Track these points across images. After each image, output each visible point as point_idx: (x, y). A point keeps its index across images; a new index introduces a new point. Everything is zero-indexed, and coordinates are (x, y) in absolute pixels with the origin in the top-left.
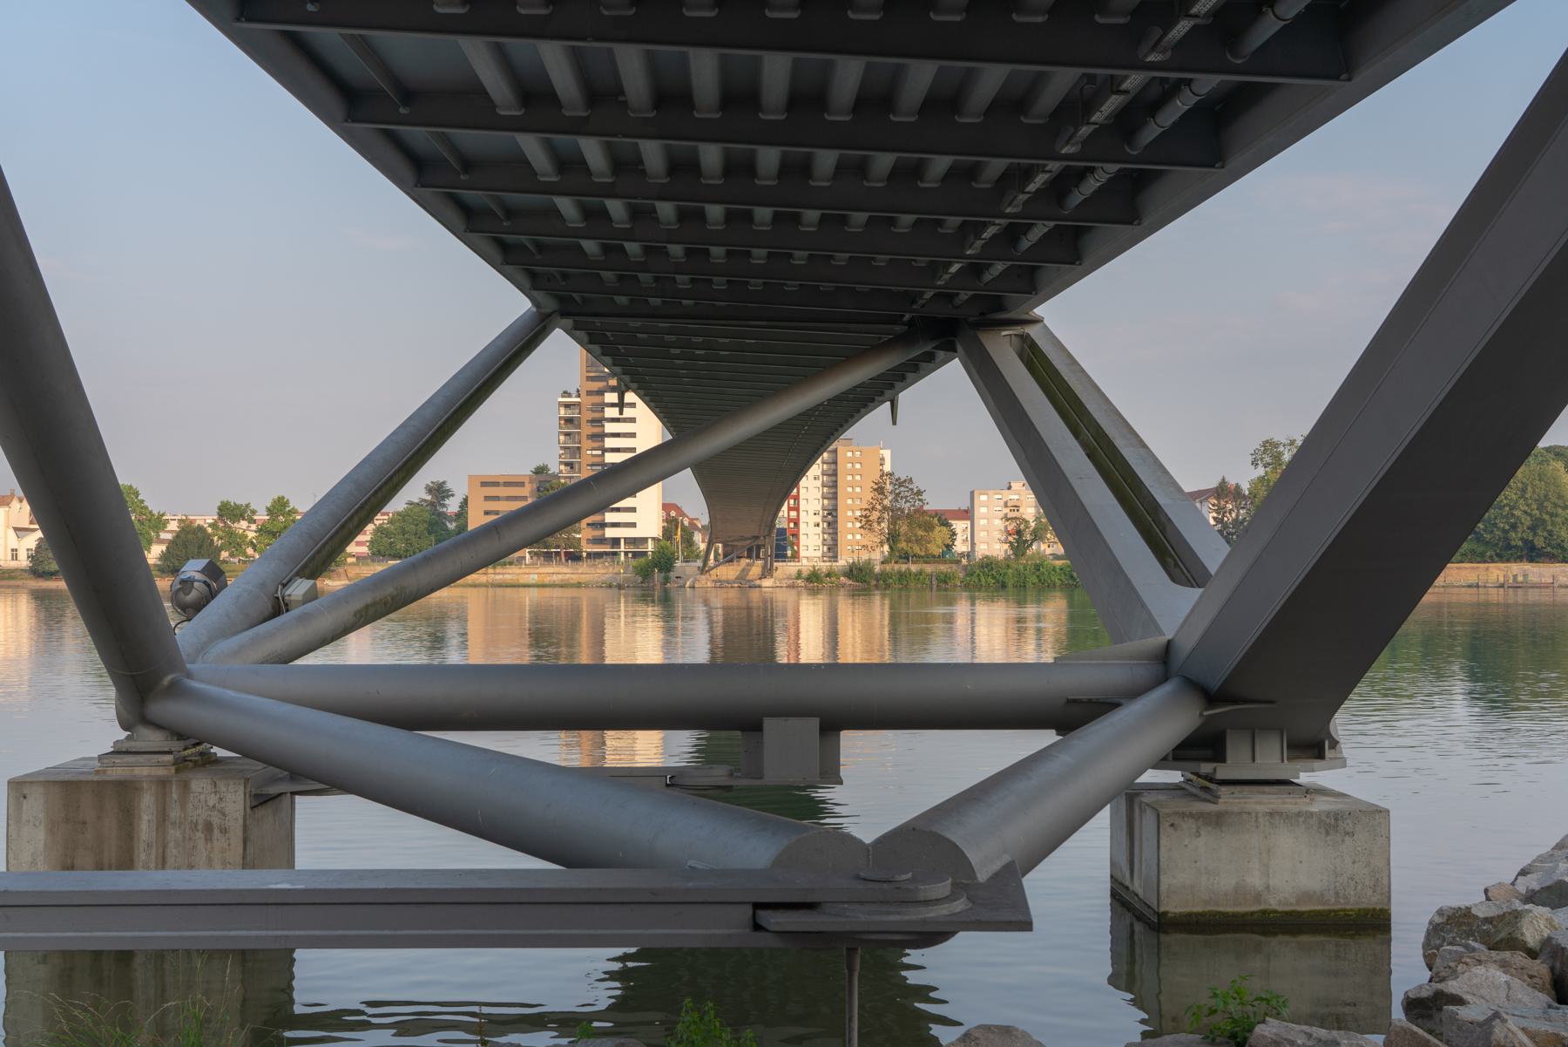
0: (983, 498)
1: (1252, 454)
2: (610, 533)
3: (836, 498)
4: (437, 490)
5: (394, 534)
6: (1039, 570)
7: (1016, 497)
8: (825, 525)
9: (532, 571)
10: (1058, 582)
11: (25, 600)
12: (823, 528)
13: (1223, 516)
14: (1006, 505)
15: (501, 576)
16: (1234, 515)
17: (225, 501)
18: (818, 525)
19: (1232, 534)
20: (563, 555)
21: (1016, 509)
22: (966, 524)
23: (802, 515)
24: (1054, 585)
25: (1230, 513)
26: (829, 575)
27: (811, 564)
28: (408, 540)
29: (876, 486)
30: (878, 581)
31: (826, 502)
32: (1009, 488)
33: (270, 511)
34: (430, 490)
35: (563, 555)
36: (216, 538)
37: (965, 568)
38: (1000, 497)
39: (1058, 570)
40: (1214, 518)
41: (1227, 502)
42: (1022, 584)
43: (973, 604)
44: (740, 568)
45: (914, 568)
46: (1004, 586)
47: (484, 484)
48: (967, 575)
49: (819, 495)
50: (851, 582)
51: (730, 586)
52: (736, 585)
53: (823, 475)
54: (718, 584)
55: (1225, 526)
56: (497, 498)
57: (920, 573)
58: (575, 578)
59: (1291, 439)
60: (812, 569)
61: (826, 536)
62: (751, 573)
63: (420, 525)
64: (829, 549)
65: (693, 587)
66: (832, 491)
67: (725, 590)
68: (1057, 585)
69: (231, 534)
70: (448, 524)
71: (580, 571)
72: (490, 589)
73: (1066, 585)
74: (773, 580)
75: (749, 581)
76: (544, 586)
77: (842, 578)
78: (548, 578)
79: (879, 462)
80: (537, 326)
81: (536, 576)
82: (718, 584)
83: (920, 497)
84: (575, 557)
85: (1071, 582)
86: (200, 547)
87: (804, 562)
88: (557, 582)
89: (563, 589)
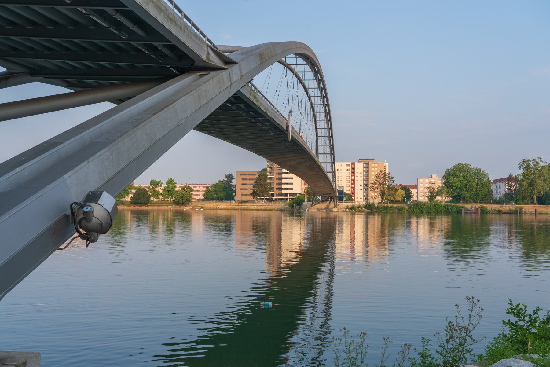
0: (422, 180)
1: (519, 164)
2: (284, 192)
3: (368, 180)
4: (229, 177)
5: (212, 192)
6: (436, 206)
7: (434, 180)
8: (364, 190)
9: (254, 205)
10: (443, 211)
11: (377, 216)
12: (364, 191)
13: (511, 187)
14: (430, 183)
15: (243, 206)
16: (515, 187)
17: (153, 179)
18: (362, 190)
19: (514, 194)
20: (265, 199)
21: (434, 184)
22: (416, 190)
23: (356, 186)
24: (441, 212)
25: (513, 187)
26: (358, 207)
27: (359, 203)
28: (216, 194)
29: (376, 176)
30: (376, 209)
31: (365, 182)
32: (431, 177)
33: (167, 183)
34: (227, 177)
35: (265, 199)
36: (149, 192)
37: (408, 205)
38: (428, 180)
39: (443, 207)
40: (507, 188)
41: (512, 183)
42: (429, 212)
43: (417, 219)
44: (327, 204)
45: (389, 205)
46: (422, 212)
47: (242, 174)
48: (409, 208)
49: (362, 179)
50: (366, 210)
51: (322, 211)
52: (324, 210)
53: (364, 172)
54: (318, 210)
55: (511, 191)
56: (246, 179)
57: (392, 207)
58: (269, 207)
59: (534, 159)
60: (352, 205)
61: (364, 194)
62: (330, 206)
63: (221, 189)
64: (366, 198)
65: (308, 211)
66: (367, 178)
67: (321, 212)
68: (442, 212)
69: (154, 191)
70: (233, 188)
71: (270, 205)
72: (240, 211)
73: (446, 212)
74: (337, 209)
75: (329, 209)
76: (258, 210)
77: (363, 208)
78: (260, 207)
79: (384, 167)
80: (4, 75)
81: (255, 207)
82: (318, 210)
83: (393, 179)
84: (270, 200)
85: (448, 211)
86: (144, 195)
87: (357, 203)
88: (263, 209)
89: (265, 211)
